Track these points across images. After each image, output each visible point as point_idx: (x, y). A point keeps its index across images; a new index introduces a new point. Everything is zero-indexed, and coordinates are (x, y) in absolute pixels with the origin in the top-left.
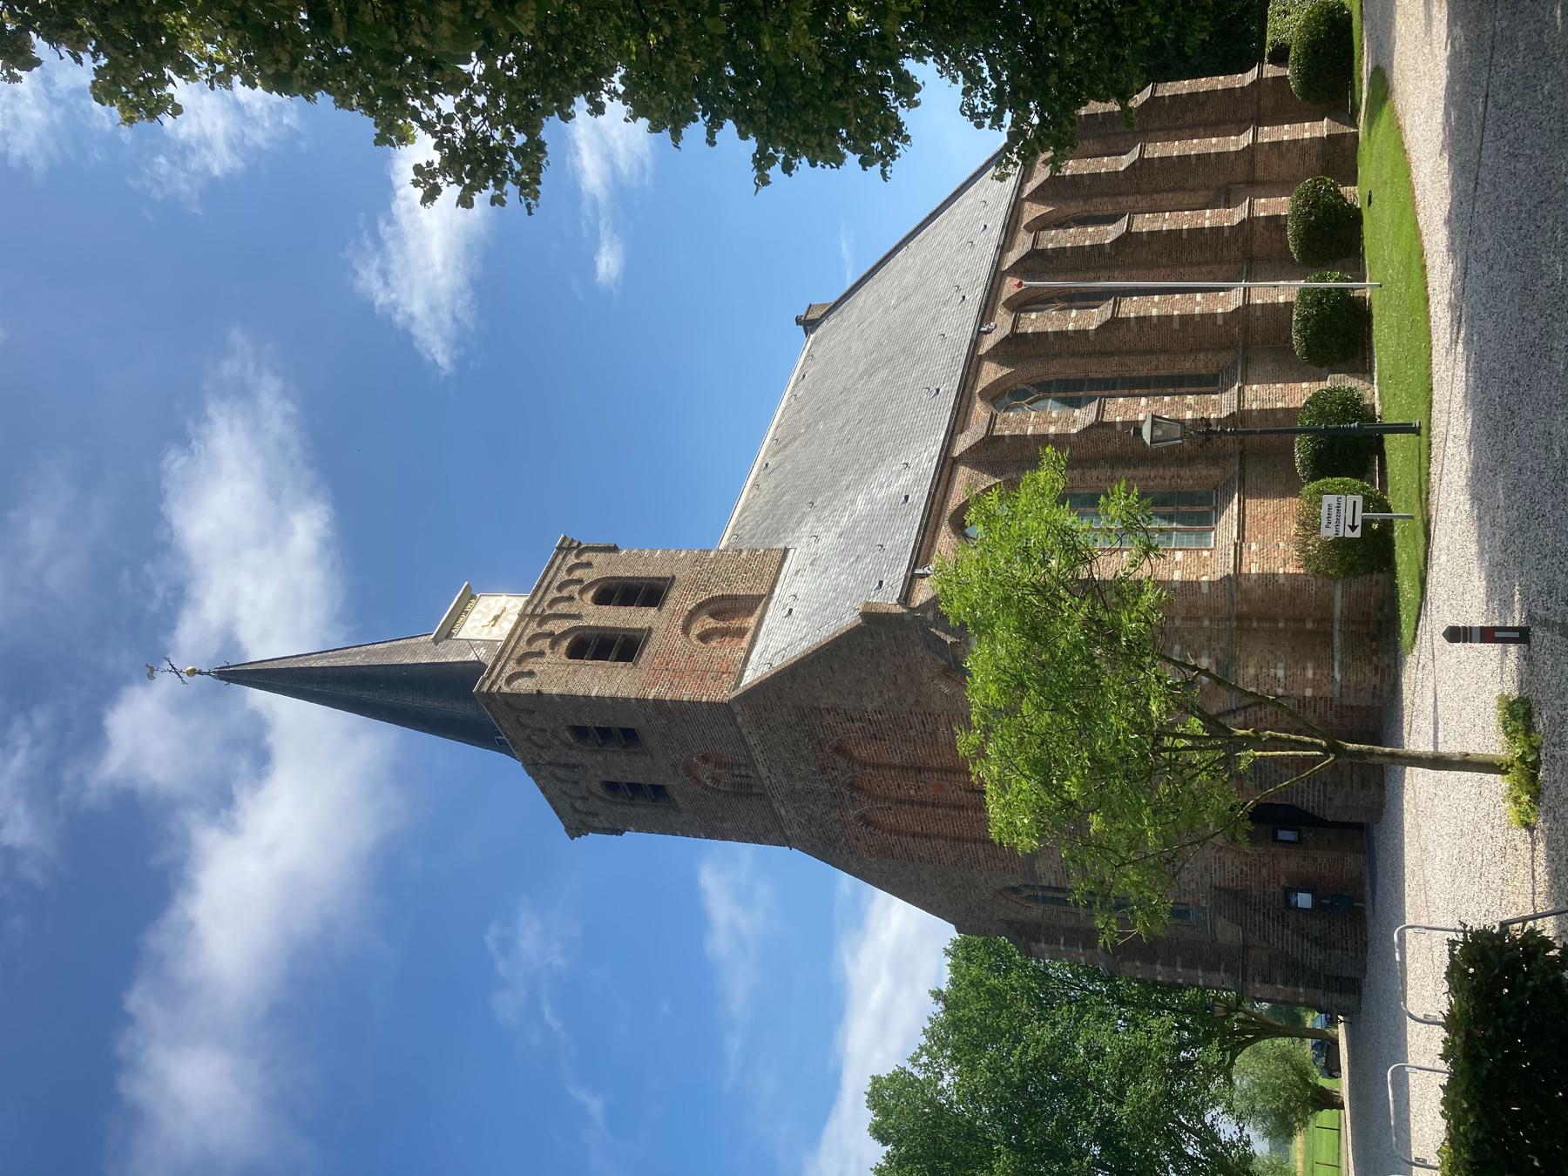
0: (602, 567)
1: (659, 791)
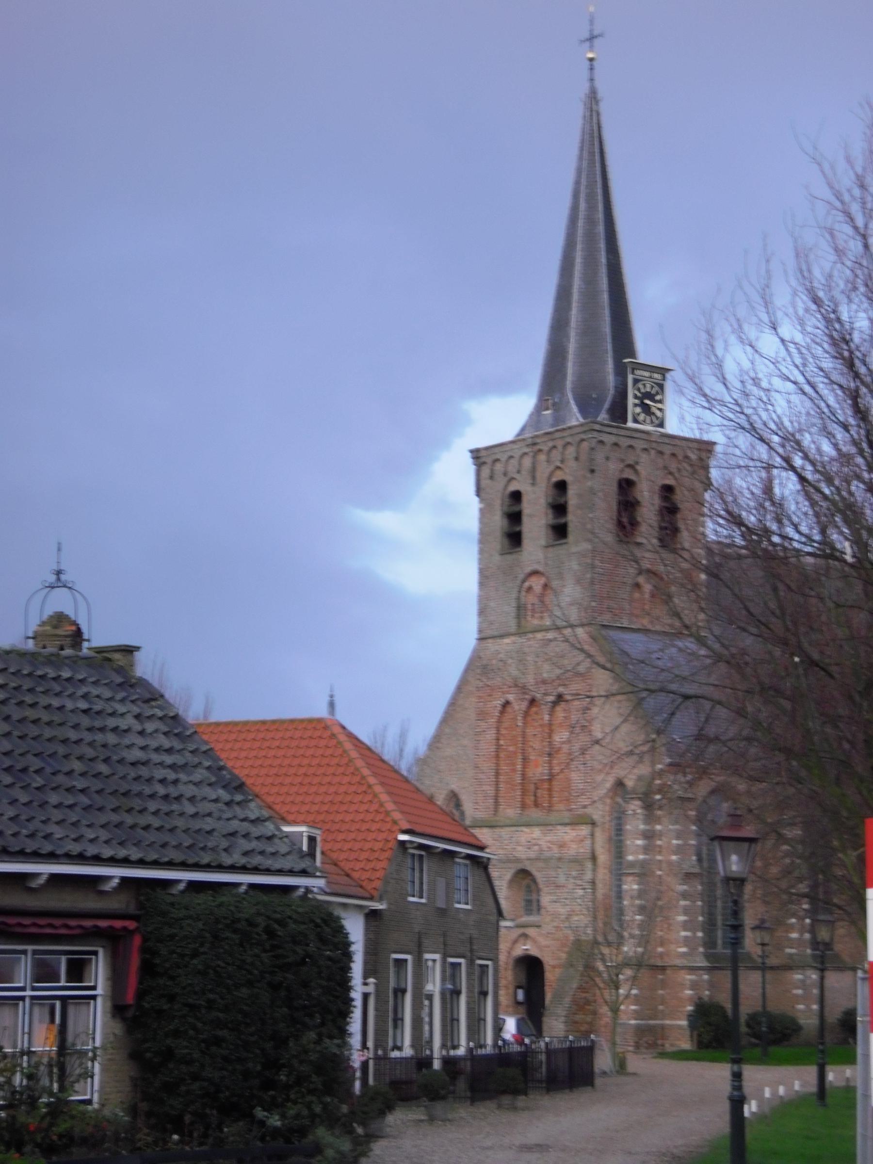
1: (514, 539)
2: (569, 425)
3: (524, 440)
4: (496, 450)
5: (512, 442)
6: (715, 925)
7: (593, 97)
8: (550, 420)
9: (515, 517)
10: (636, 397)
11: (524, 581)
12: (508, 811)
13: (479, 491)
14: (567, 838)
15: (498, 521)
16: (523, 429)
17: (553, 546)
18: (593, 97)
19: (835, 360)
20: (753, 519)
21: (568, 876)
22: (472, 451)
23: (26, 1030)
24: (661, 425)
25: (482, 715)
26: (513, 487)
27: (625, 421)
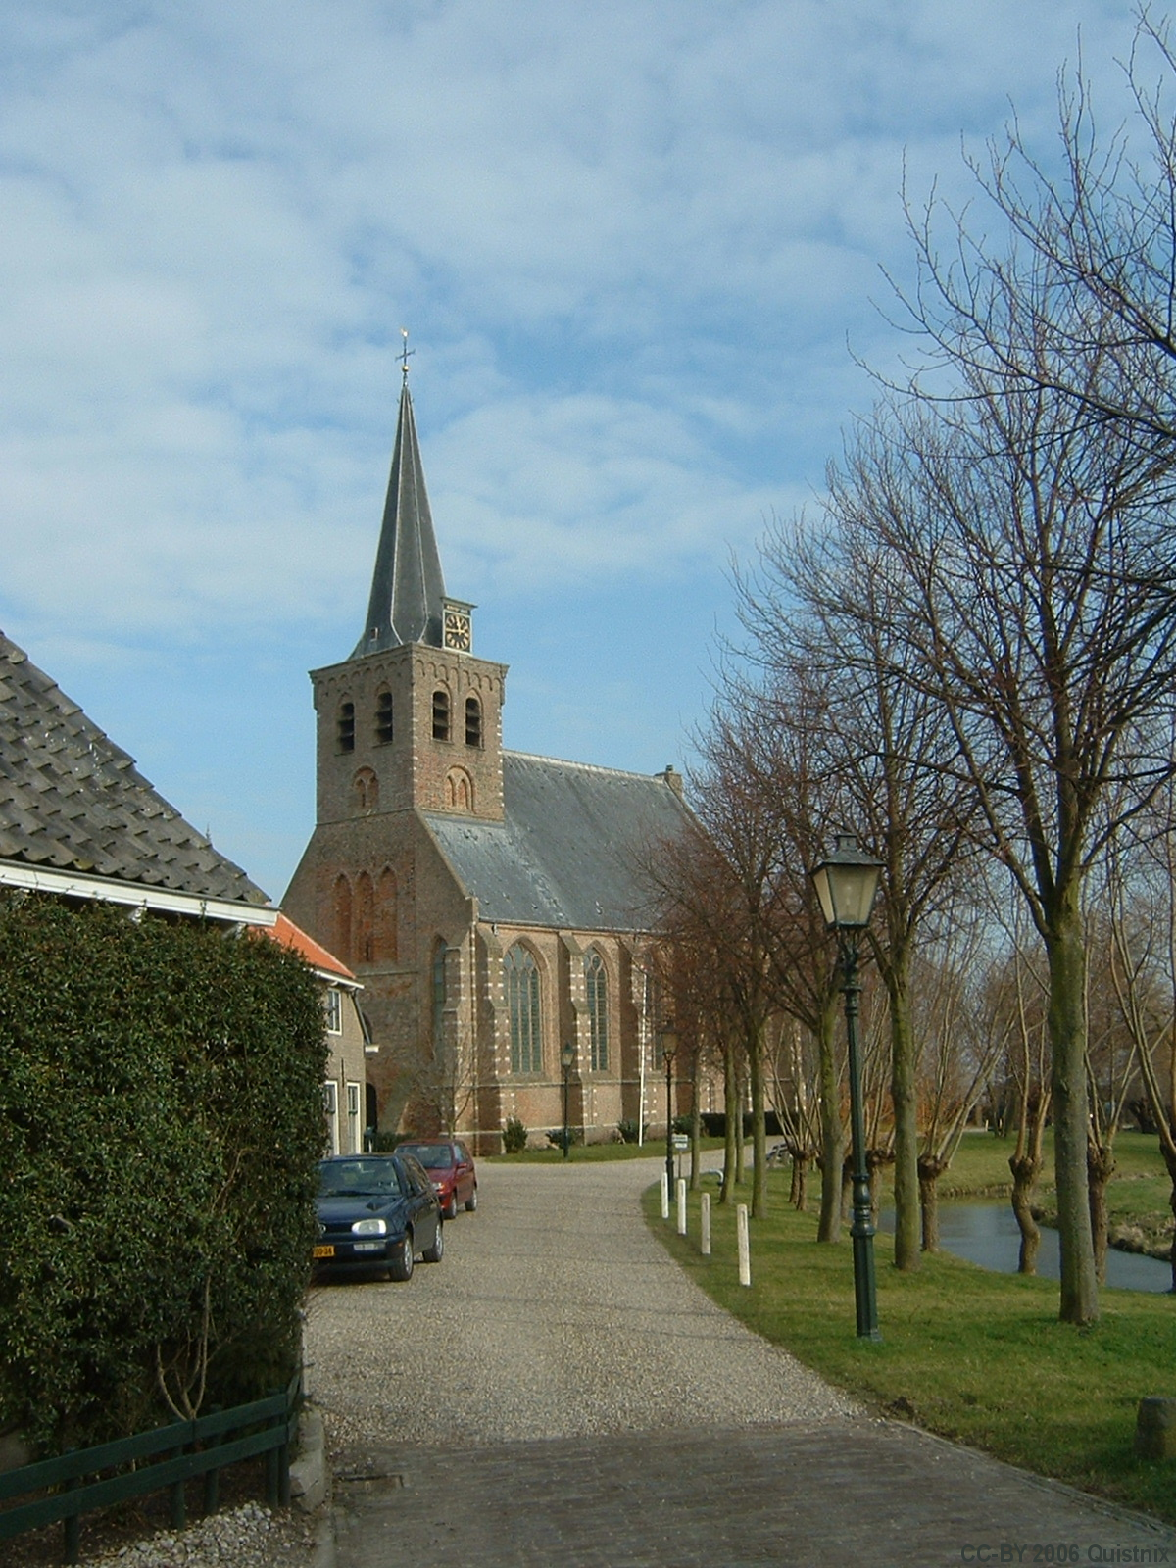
0: (486, 698)
1: (347, 743)
2: (391, 647)
3: (354, 661)
4: (332, 671)
5: (346, 663)
6: (601, 1042)
7: (405, 398)
8: (376, 646)
9: (347, 725)
10: (448, 626)
11: (355, 777)
12: (1020, 844)
13: (317, 705)
14: (394, 985)
15: (335, 731)
16: (353, 654)
17: (381, 746)
18: (405, 398)
19: (780, 578)
20: (969, 663)
21: (395, 1016)
22: (310, 673)
23: (583, 1021)
24: (468, 650)
25: (320, 888)
26: (345, 701)
27: (440, 646)
